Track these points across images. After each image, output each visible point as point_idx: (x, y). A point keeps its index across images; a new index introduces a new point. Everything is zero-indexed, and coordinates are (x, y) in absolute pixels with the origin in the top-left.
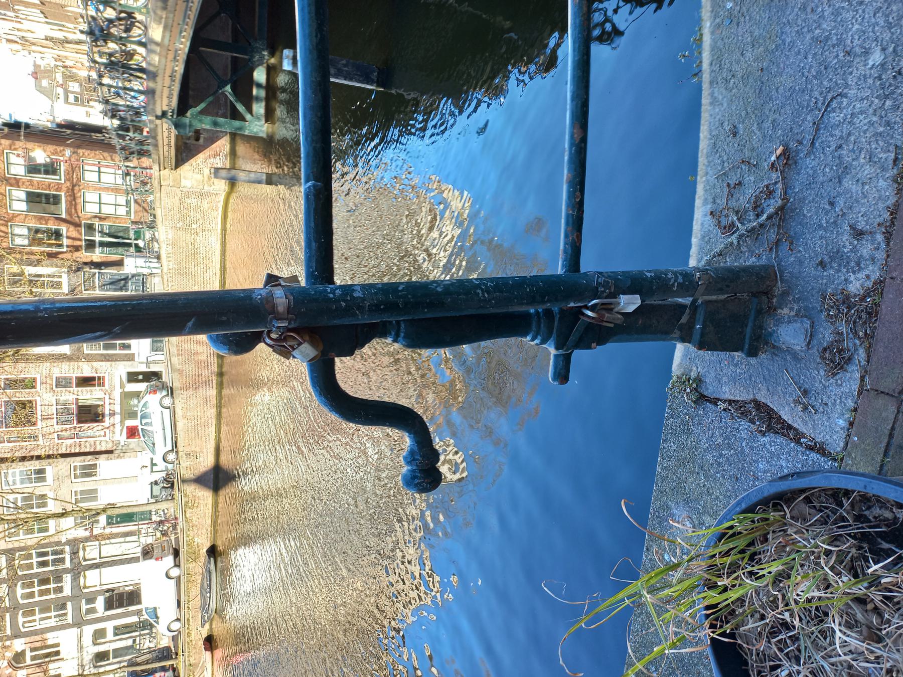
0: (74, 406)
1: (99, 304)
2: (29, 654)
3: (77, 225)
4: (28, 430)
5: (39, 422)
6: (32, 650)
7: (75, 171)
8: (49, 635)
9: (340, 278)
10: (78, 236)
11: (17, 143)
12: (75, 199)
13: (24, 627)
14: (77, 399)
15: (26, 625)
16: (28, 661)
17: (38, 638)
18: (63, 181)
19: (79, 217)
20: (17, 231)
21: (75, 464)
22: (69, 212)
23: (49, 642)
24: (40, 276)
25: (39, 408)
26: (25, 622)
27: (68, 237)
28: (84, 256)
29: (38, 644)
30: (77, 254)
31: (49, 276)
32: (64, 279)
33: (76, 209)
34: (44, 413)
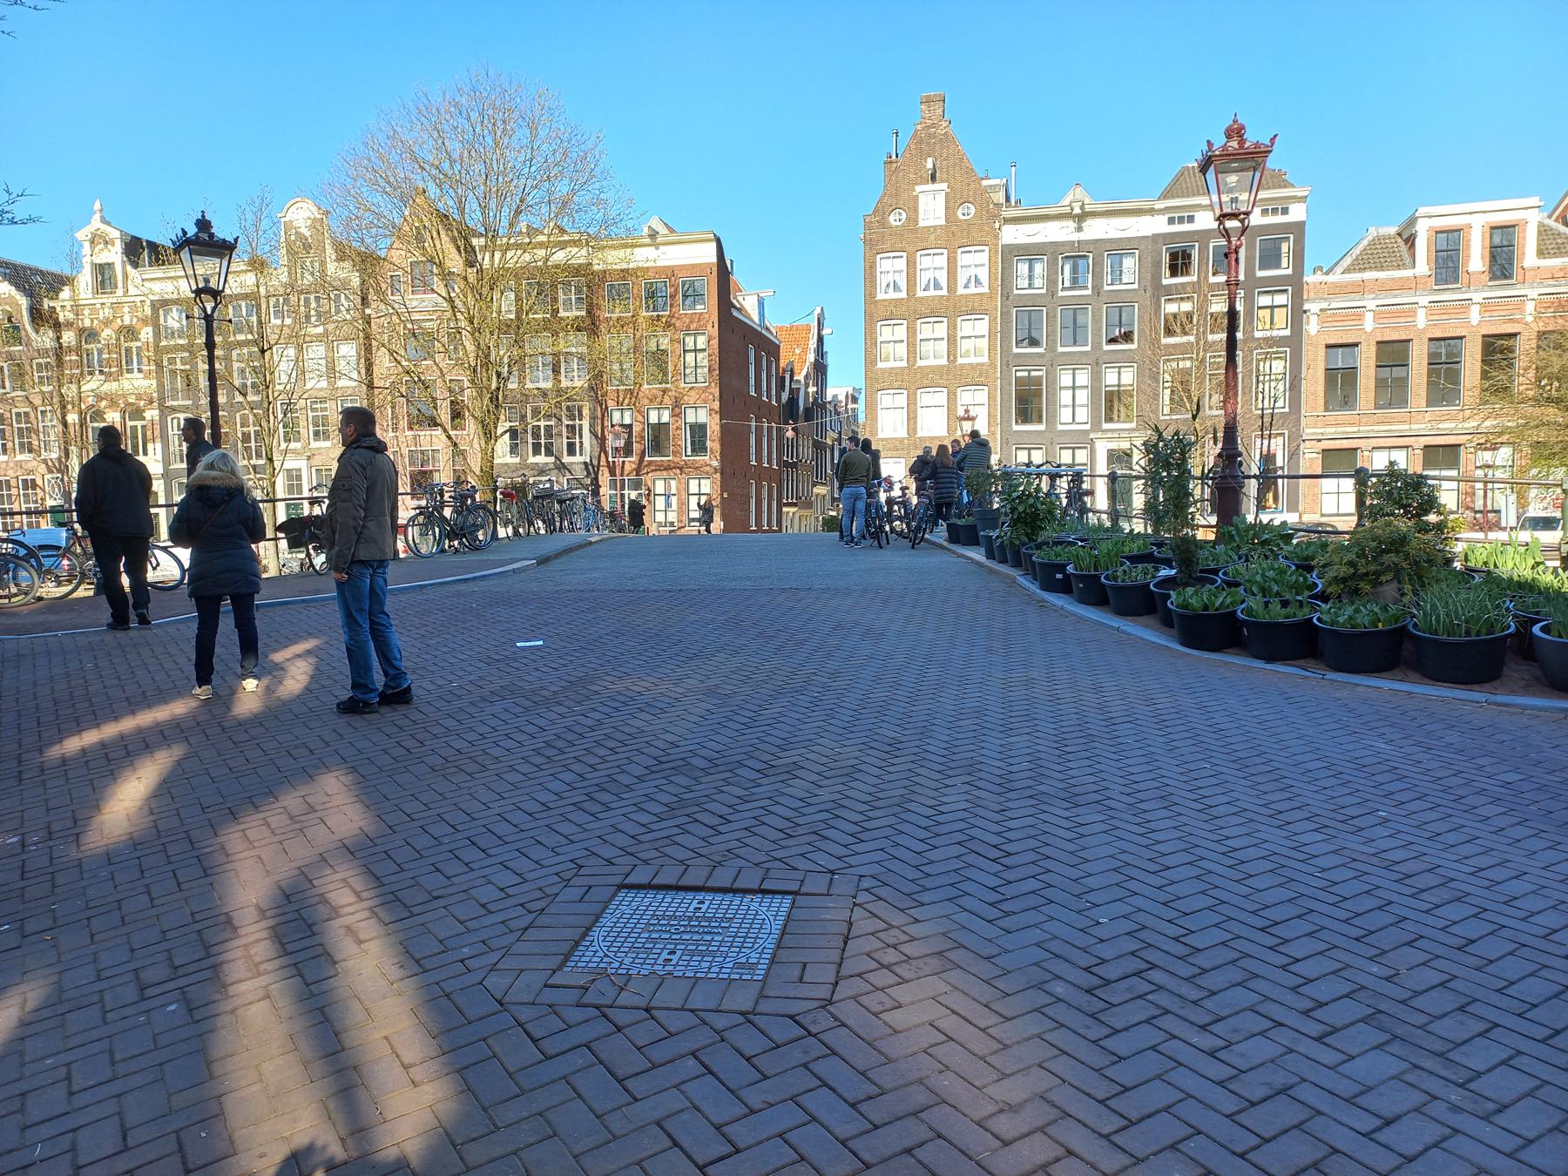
0: (431, 468)
1: (1445, 685)
2: (139, 424)
3: (638, 471)
4: (404, 423)
5: (411, 433)
6: (143, 427)
7: (699, 471)
8: (159, 446)
9: (920, 434)
10: (626, 473)
11: (717, 417)
12: (665, 469)
13: (172, 419)
14: (439, 471)
15: (175, 421)
16: (129, 423)
17: (157, 432)
18: (684, 458)
19: (648, 473)
20: (627, 415)
21: (18, 410)
22: (650, 463)
23: (150, 446)
24: (581, 437)
25: (428, 433)
26: (179, 419)
27: (624, 462)
28: (604, 478)
29: (149, 433)
30: (607, 473)
31: (581, 443)
32: (578, 459)
33: (655, 470)
34: (422, 438)
